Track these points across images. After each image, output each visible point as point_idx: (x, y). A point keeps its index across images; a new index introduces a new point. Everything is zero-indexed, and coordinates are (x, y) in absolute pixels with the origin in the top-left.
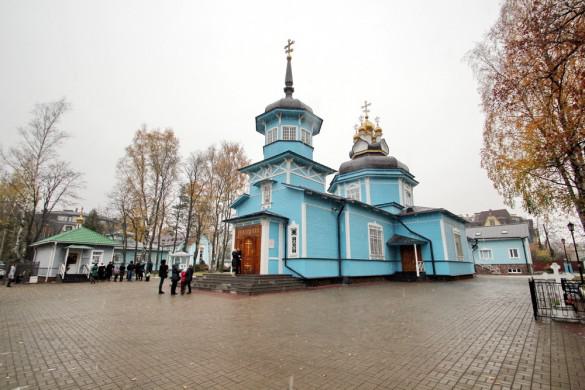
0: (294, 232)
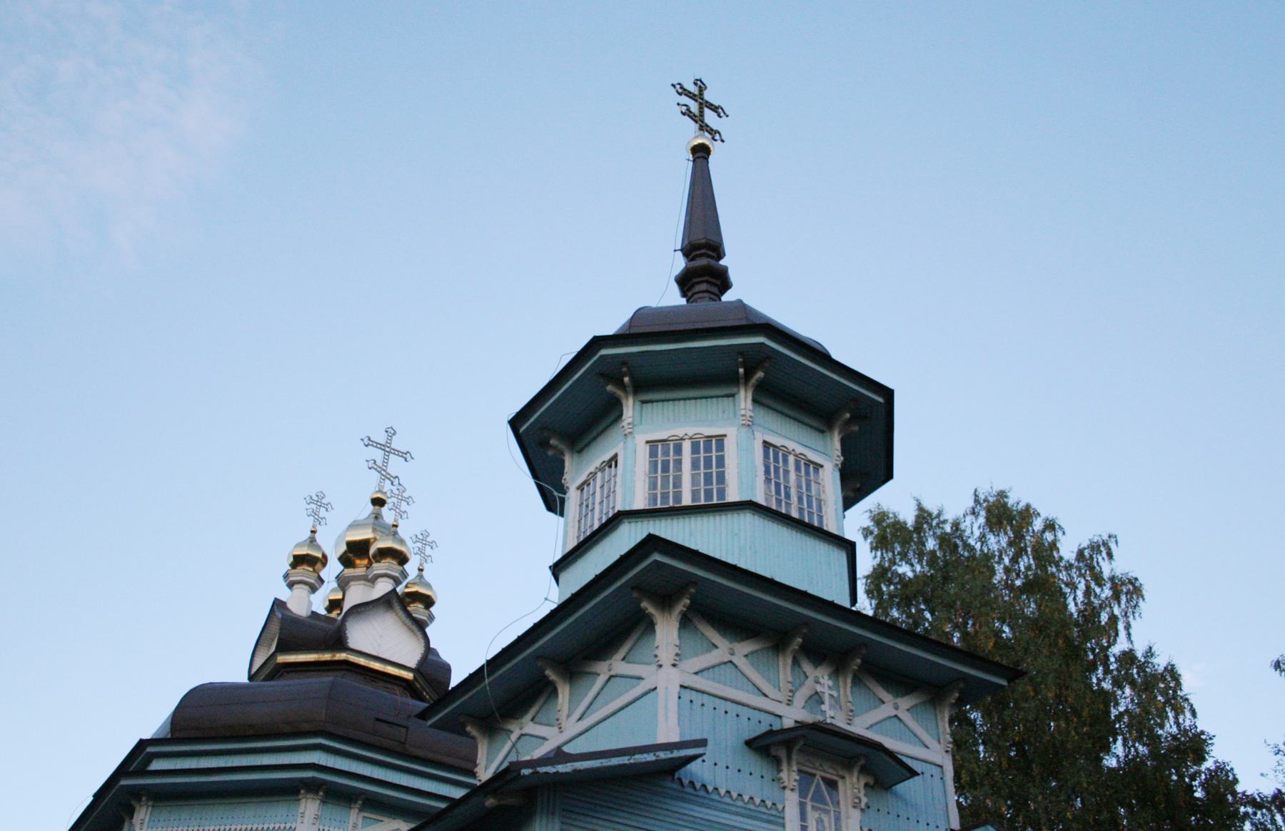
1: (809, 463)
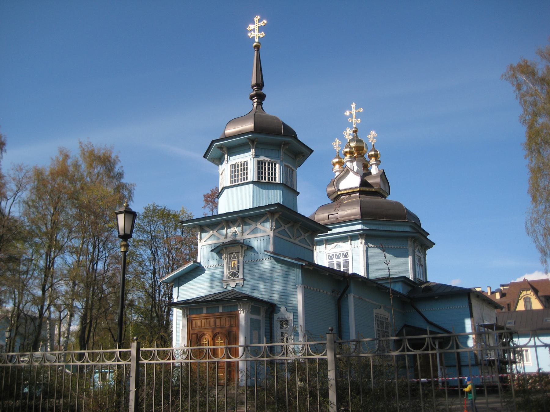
1: (292, 169)
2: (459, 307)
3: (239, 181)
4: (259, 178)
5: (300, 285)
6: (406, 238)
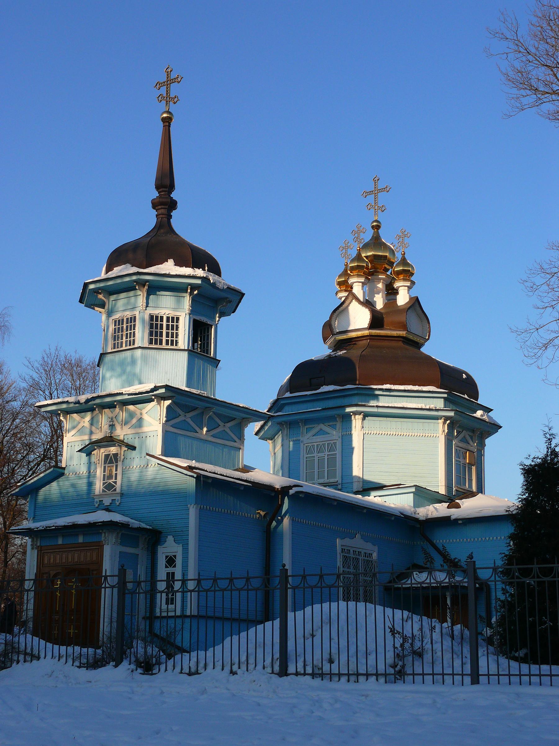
0: (171, 561)
2: (491, 538)
3: (124, 345)
4: (151, 343)
5: (193, 505)
6: (437, 418)
